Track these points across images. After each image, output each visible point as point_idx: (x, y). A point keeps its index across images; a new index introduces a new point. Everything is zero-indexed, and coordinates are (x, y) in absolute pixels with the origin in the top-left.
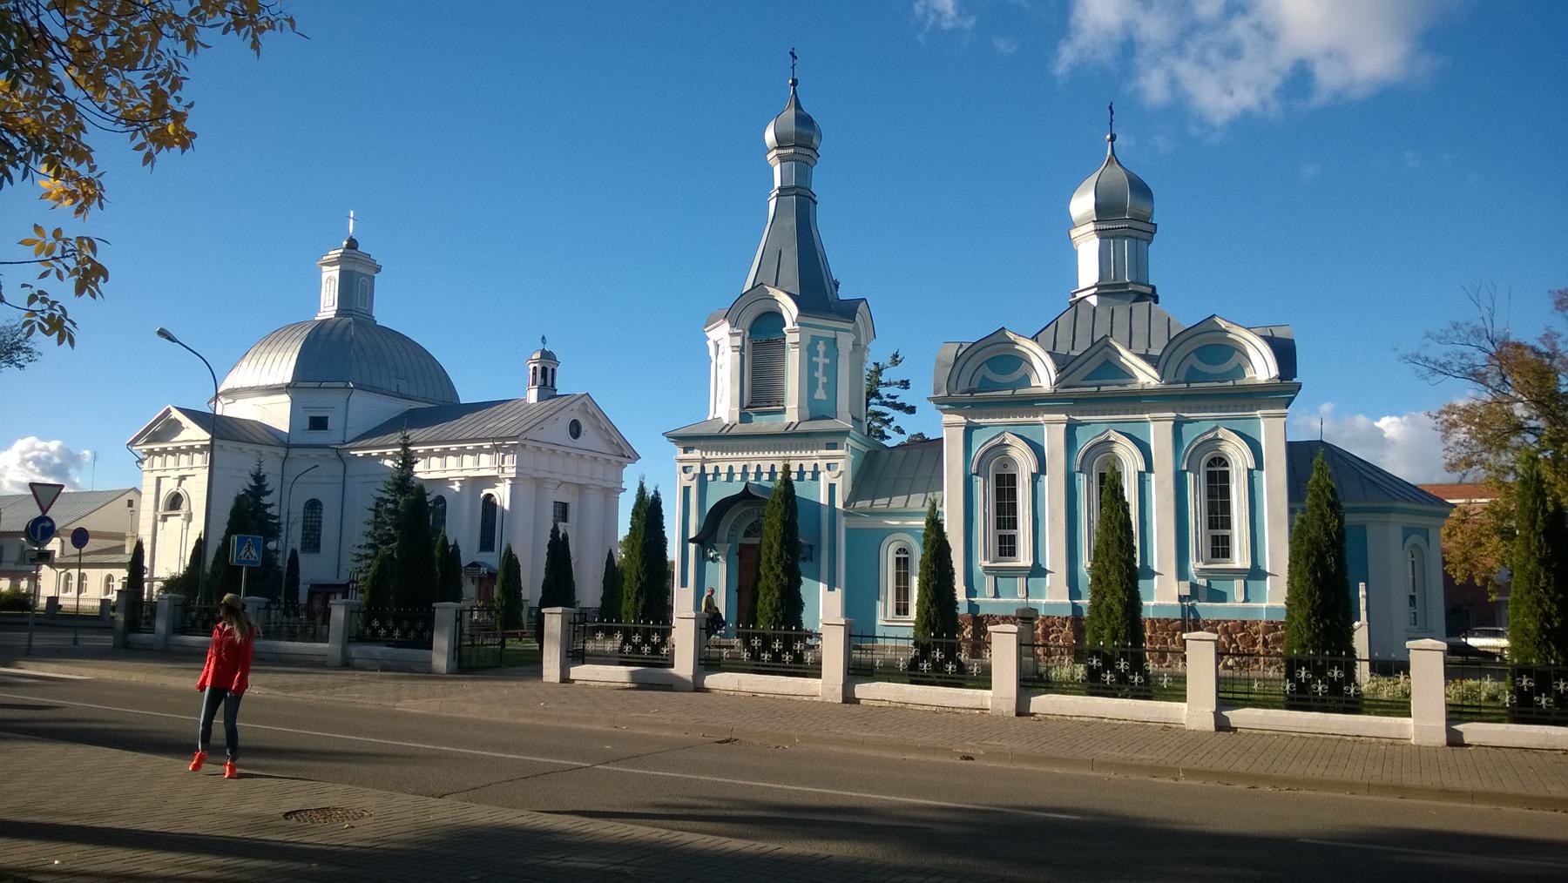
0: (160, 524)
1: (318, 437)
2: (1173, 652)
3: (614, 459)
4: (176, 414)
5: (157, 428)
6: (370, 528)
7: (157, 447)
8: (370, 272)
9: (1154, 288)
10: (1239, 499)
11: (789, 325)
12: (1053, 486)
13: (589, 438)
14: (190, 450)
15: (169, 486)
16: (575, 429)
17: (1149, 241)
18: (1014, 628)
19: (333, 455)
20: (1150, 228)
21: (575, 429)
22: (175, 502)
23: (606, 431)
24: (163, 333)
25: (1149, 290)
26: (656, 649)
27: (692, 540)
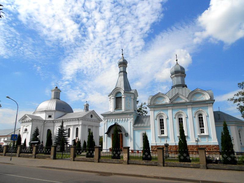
0: (23, 134)
1: (50, 119)
2: (195, 152)
3: (98, 121)
4: (26, 116)
5: (23, 118)
6: (35, 130)
7: (23, 121)
8: (59, 92)
9: (186, 85)
10: (205, 120)
11: (122, 94)
12: (170, 121)
13: (94, 118)
14: (29, 122)
15: (25, 128)
16: (92, 116)
17: (185, 77)
18: (214, 141)
19: (52, 122)
20: (185, 75)
21: (92, 116)
22: (26, 130)
23: (95, 114)
24: (8, 97)
25: (185, 86)
26: (91, 154)
27: (105, 133)
